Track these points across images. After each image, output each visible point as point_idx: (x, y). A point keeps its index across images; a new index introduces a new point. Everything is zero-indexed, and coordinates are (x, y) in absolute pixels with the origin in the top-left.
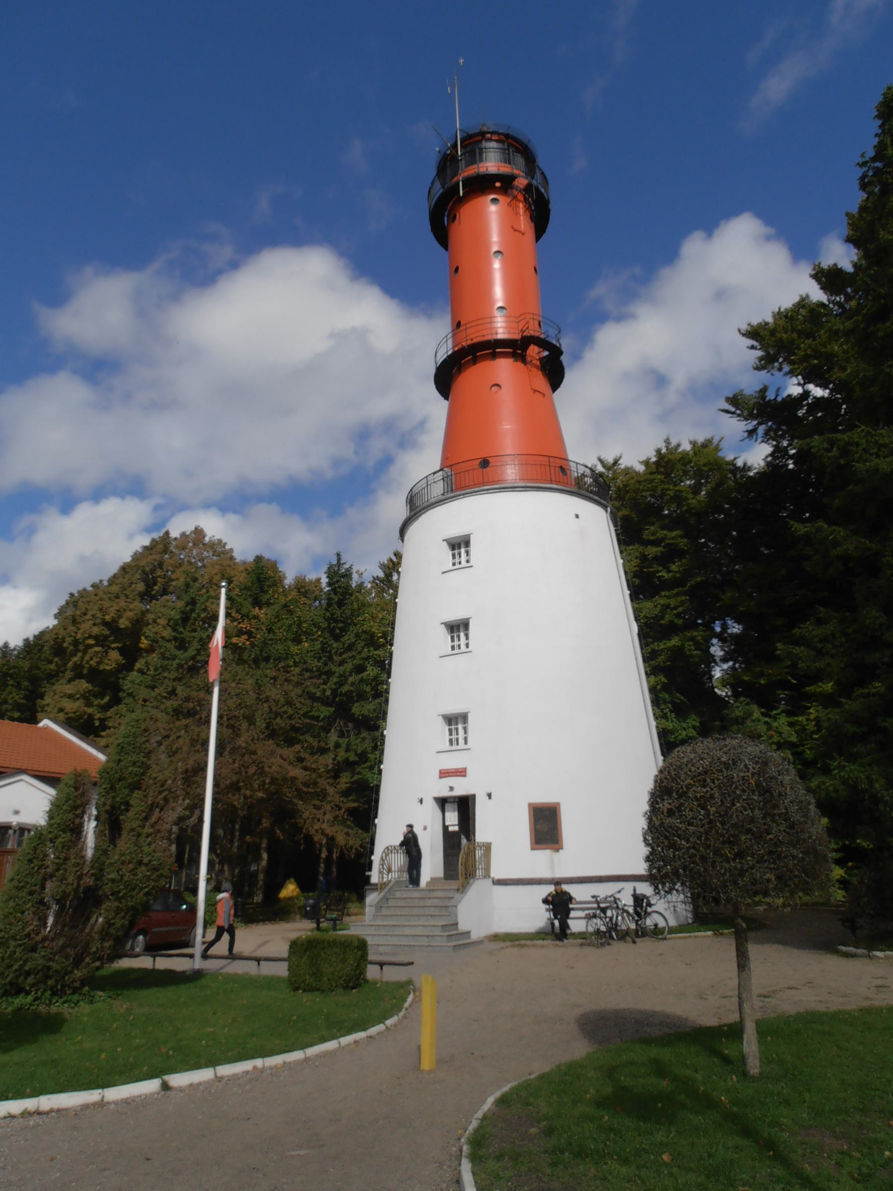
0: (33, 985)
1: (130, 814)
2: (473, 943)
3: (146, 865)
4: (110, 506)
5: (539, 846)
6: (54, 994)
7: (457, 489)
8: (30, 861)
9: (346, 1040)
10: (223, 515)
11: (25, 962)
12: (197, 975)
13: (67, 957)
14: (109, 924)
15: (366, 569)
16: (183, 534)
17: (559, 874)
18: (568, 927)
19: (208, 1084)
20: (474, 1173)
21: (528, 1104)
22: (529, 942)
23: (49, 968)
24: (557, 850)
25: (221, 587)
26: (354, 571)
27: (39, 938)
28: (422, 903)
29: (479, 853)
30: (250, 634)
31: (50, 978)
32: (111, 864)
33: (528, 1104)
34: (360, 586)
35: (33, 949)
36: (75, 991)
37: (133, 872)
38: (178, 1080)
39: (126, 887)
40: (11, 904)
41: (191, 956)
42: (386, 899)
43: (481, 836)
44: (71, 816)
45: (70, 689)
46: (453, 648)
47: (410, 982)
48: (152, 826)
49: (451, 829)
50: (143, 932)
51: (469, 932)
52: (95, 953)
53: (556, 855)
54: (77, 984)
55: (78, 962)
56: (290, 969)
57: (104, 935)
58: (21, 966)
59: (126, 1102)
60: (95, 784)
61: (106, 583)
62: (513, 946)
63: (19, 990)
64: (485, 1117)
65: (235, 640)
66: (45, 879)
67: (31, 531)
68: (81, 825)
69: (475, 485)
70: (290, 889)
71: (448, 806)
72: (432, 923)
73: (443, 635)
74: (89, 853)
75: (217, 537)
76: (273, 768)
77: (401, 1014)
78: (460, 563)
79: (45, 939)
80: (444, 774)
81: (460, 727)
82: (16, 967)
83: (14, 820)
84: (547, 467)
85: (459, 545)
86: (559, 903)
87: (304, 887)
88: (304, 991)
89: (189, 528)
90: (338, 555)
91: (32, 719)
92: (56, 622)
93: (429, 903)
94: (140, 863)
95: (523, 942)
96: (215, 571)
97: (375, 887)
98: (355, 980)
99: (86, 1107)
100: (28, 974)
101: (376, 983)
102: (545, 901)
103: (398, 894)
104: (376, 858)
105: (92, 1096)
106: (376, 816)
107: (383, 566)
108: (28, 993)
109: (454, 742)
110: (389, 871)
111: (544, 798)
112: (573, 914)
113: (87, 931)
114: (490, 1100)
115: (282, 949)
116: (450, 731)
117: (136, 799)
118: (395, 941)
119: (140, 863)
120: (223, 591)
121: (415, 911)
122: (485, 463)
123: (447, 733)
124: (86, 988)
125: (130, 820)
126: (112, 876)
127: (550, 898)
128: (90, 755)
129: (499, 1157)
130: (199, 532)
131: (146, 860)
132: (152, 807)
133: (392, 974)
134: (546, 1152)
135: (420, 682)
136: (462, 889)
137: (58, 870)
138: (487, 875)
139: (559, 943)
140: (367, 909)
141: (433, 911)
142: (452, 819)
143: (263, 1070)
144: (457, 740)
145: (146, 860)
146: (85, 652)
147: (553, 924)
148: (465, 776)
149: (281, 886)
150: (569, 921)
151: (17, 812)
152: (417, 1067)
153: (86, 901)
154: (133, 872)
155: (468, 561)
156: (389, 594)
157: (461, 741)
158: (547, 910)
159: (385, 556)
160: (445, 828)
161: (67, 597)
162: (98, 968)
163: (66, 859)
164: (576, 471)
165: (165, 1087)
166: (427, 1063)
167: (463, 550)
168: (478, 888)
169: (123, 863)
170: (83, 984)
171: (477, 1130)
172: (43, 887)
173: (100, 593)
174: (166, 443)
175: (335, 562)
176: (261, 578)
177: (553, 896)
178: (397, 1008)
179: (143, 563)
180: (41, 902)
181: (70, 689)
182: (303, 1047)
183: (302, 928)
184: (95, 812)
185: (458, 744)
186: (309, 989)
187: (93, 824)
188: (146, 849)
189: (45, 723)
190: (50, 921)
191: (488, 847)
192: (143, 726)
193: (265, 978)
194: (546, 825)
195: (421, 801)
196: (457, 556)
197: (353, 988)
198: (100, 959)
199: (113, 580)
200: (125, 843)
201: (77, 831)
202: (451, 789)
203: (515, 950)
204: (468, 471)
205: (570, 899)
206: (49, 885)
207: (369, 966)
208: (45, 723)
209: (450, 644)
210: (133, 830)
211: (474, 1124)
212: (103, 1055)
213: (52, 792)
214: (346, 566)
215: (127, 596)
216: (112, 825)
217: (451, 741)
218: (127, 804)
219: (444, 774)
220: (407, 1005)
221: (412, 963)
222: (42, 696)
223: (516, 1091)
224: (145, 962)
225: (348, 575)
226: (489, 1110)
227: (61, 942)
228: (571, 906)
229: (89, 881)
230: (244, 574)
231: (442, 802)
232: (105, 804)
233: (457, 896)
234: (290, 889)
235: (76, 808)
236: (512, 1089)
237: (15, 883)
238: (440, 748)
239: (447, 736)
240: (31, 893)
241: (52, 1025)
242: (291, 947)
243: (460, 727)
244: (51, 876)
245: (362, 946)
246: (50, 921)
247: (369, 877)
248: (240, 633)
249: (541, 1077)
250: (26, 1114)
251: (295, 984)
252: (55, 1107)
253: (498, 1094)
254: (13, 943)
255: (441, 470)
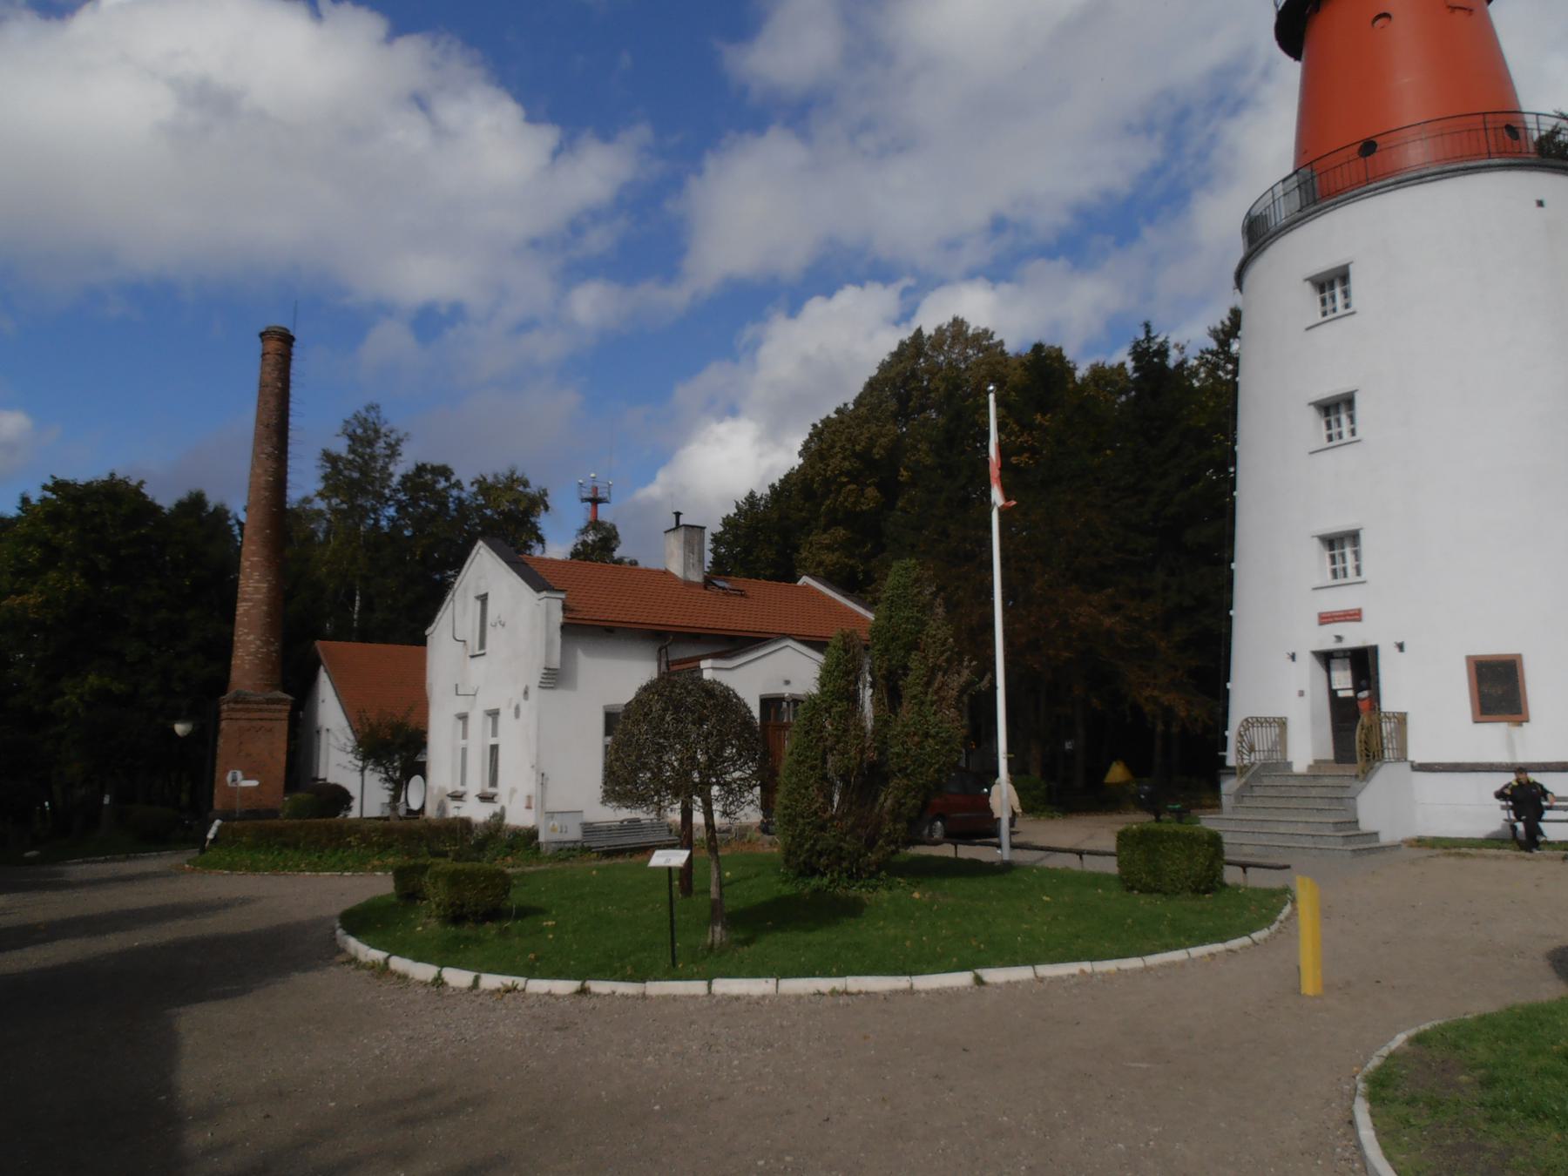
0: (827, 867)
1: (910, 679)
2: (1383, 848)
3: (934, 737)
4: (848, 297)
5: (1486, 717)
6: (850, 877)
7: (1324, 197)
8: (807, 733)
9: (1197, 951)
10: (993, 288)
11: (816, 841)
12: (1007, 867)
13: (859, 838)
14: (899, 803)
15: (1189, 339)
16: (939, 330)
17: (1522, 758)
18: (1541, 833)
19: (1028, 983)
20: (1372, 1115)
21: (1457, 1047)
22: (1473, 851)
23: (841, 849)
24: (1520, 723)
25: (988, 393)
26: (1171, 343)
27: (827, 816)
28: (1302, 793)
29: (1387, 728)
30: (1033, 451)
31: (843, 859)
32: (895, 737)
33: (1457, 1047)
34: (1181, 365)
35: (822, 828)
36: (872, 875)
37: (920, 745)
38: (995, 975)
39: (914, 763)
40: (794, 779)
41: (999, 846)
42: (1249, 786)
43: (1388, 704)
44: (843, 683)
45: (826, 539)
46: (1330, 438)
47: (1286, 891)
48: (936, 693)
49: (1341, 694)
50: (942, 817)
51: (1376, 834)
52: (888, 835)
53: (1516, 731)
54: (873, 868)
55: (871, 844)
56: (1120, 864)
57: (896, 816)
58: (813, 846)
59: (939, 992)
60: (867, 648)
61: (851, 407)
62: (1450, 855)
63: (814, 872)
64: (1391, 1056)
65: (1014, 460)
66: (825, 753)
67: (756, 344)
68: (857, 692)
69: (1353, 186)
70: (1117, 773)
71: (1335, 663)
72: (1318, 819)
73: (1313, 425)
74: (869, 724)
75: (983, 326)
76: (1082, 619)
77: (1274, 928)
78: (1334, 310)
79: (833, 818)
80: (1326, 619)
81: (1348, 551)
82: (807, 846)
83: (786, 691)
84: (1482, 133)
85: (1331, 283)
86: (1526, 799)
87: (1138, 769)
88: (1141, 891)
89: (945, 319)
90: (1147, 326)
91: (788, 575)
92: (801, 461)
93: (1314, 792)
94: (927, 735)
95: (1464, 850)
96: (982, 372)
97: (1232, 771)
98: (1209, 883)
99: (895, 993)
100: (820, 854)
101: (1238, 887)
102: (1500, 795)
103: (1266, 781)
104: (1232, 734)
105: (901, 982)
106: (1230, 607)
107: (1214, 334)
108: (823, 875)
109: (1340, 573)
110: (1252, 749)
111: (1494, 646)
112: (1548, 815)
113: (877, 810)
114: (1400, 1039)
115: (1110, 843)
116: (1333, 557)
117: (914, 660)
118: (1264, 840)
119: (927, 735)
120: (992, 397)
121: (1293, 803)
122: (1368, 147)
123: (1328, 560)
124: (883, 873)
125: (911, 685)
126: (896, 750)
127: (1508, 792)
128: (858, 615)
129: (1411, 1102)
130: (958, 323)
131: (933, 732)
132: (933, 671)
133: (1258, 879)
134: (1482, 1104)
135: (1283, 492)
136: (1365, 775)
137: (838, 742)
138: (1402, 756)
139: (1527, 854)
140: (1224, 799)
141: (1320, 804)
142: (1343, 680)
143: (1092, 975)
144: (1345, 570)
145: (933, 732)
146: (839, 492)
147: (1514, 828)
148: (1359, 620)
149: (1105, 770)
150: (1542, 825)
151: (787, 682)
152: (1297, 990)
153: (868, 780)
154: (920, 745)
155: (1347, 306)
156: (1227, 373)
157: (1351, 571)
158: (1503, 808)
159: (1220, 316)
160: (1333, 693)
161: (809, 429)
162: (893, 853)
163: (846, 731)
164: (1535, 129)
165: (979, 981)
166: (1310, 986)
167: (1338, 290)
168: (1387, 776)
169: (907, 735)
170: (879, 870)
171: (1379, 1069)
172: (825, 762)
173: (846, 419)
174: (906, 204)
175: (1142, 337)
176: (1045, 365)
177: (1513, 789)
178: (1268, 920)
179: (892, 374)
180: (824, 777)
181: (826, 539)
182: (1141, 953)
183: (1138, 820)
184: (869, 679)
185: (1345, 575)
186: (1147, 890)
187: (869, 692)
188: (931, 719)
189: (805, 580)
190: (836, 798)
191: (1401, 720)
192: (914, 575)
193: (1092, 874)
194: (1498, 688)
195: (1293, 657)
196: (1329, 301)
197: (1205, 892)
198: (895, 842)
199: (859, 402)
200: (907, 712)
201: (854, 698)
202: (1339, 638)
203: (1452, 860)
204: (1339, 164)
205: (1544, 793)
206: (830, 759)
207: (1226, 868)
208: (805, 580)
209: (1324, 432)
210: (915, 697)
211: (1375, 1062)
212: (908, 943)
213: (821, 658)
214: (1160, 340)
215: (878, 420)
216: (891, 693)
217: (1334, 572)
218: (906, 668)
219: (1326, 619)
220: (1281, 917)
221: (1287, 867)
222: (796, 549)
223: (1440, 1031)
224: (946, 850)
225: (1163, 352)
226: (1399, 1048)
227: (850, 821)
228: (1545, 803)
229: (872, 755)
230: (1020, 371)
231: (1326, 659)
232: (880, 668)
233: (1356, 784)
234: (1117, 773)
235: (848, 673)
236: (1435, 1028)
237: (795, 757)
238: (1318, 583)
239: (1328, 566)
240: (813, 768)
241: (854, 909)
242: (1119, 839)
243: (1348, 551)
244: (832, 749)
245: (1215, 841)
246: (836, 798)
247: (1224, 758)
248: (1020, 450)
249: (1482, 1018)
250: (834, 992)
251: (1128, 882)
252: (864, 989)
253: (1412, 1032)
254: (801, 821)
255: (1296, 172)
